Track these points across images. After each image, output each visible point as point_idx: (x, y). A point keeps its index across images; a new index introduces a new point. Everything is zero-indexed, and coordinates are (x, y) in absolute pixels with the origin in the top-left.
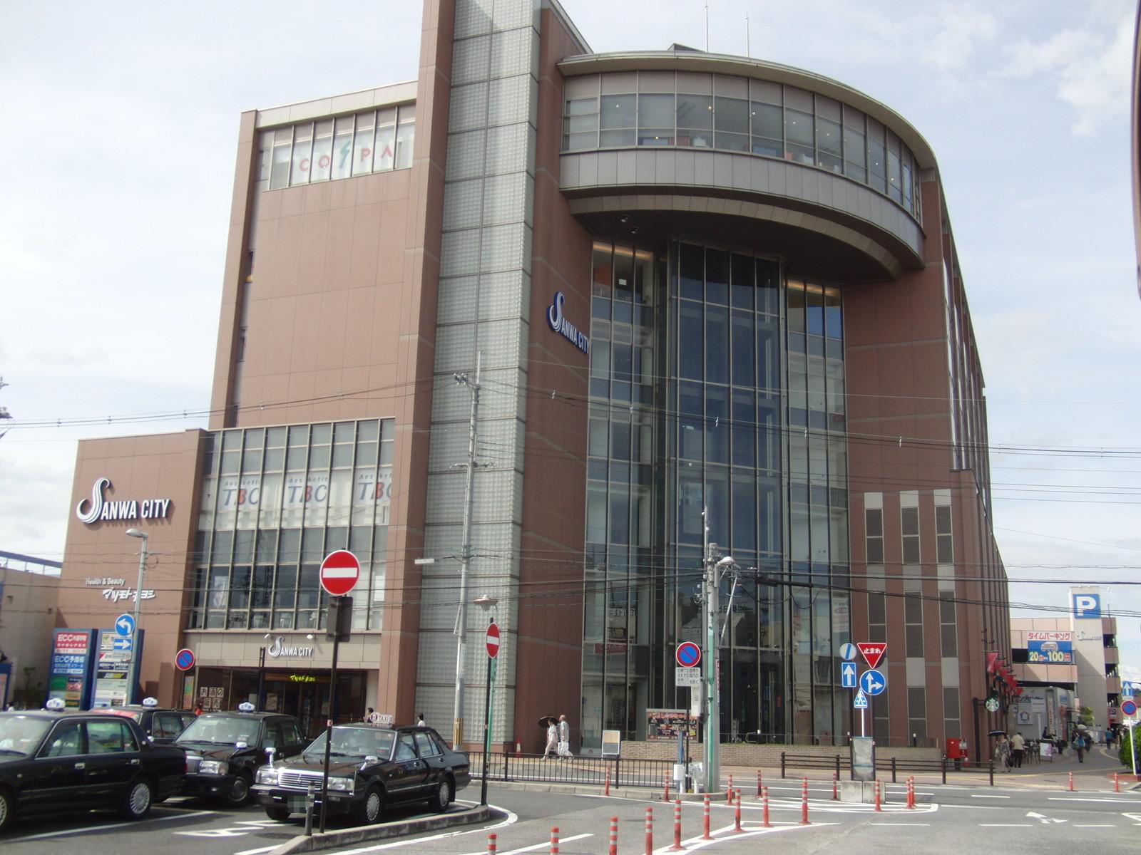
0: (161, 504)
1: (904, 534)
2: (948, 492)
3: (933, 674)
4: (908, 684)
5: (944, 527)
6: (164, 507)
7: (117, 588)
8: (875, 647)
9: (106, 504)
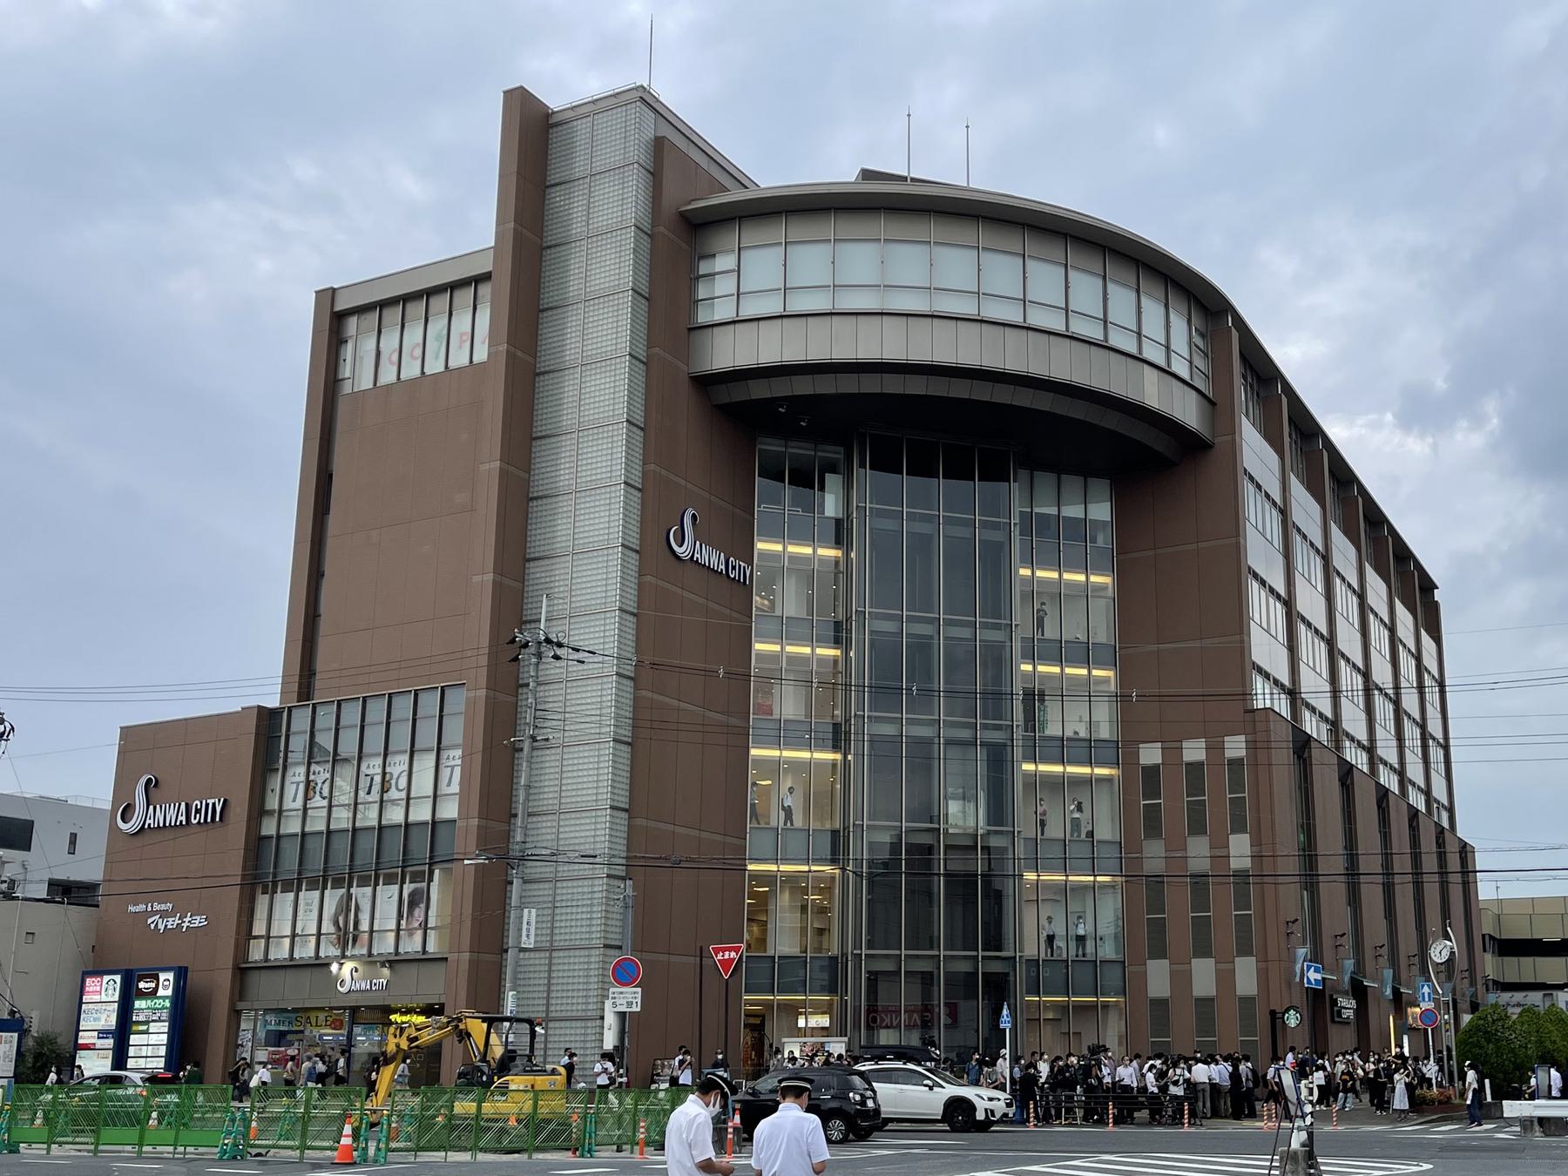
0: (214, 804)
1: (1245, 797)
2: (1201, 743)
3: (1226, 978)
4: (1194, 994)
5: (1236, 785)
6: (218, 809)
7: (164, 915)
8: (730, 949)
9: (151, 807)
